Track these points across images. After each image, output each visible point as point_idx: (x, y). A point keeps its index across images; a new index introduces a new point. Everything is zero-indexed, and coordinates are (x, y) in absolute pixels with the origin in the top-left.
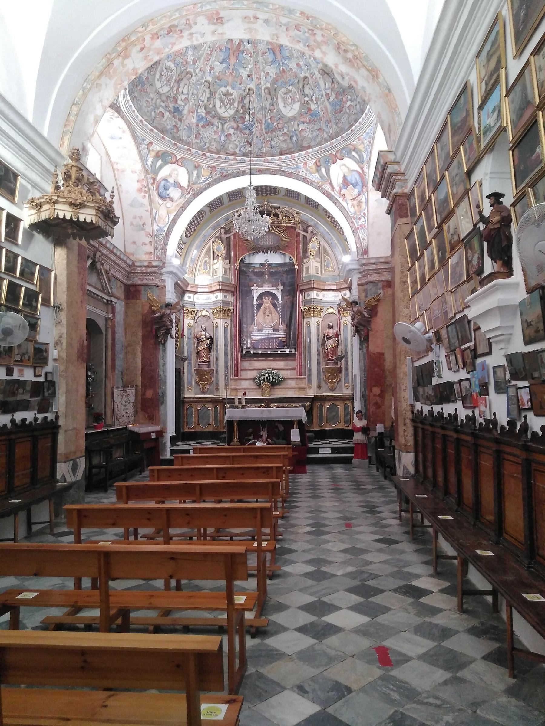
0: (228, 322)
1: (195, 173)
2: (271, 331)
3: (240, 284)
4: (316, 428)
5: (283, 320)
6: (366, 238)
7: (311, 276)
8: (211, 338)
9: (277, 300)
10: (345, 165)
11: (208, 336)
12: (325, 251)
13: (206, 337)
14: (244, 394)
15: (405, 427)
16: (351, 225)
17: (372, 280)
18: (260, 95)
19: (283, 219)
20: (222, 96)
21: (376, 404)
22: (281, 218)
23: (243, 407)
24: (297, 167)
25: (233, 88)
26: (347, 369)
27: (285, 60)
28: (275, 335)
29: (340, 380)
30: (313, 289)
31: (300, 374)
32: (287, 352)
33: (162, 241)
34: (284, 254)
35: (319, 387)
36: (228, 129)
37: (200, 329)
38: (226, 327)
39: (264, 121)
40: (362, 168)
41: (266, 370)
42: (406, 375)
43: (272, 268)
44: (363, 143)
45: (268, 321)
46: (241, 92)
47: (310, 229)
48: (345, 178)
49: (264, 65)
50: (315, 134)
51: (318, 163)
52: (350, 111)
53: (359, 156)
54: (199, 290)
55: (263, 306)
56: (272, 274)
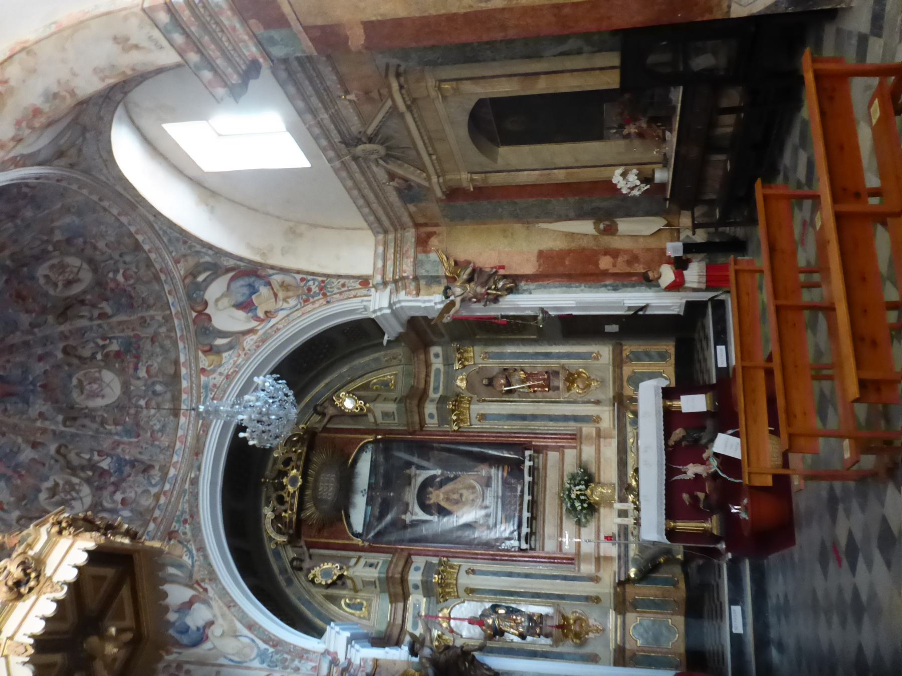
5: (470, 469)
10: (217, 300)
18: (73, 436)
20: (54, 499)
21: (629, 263)
25: (46, 479)
27: (26, 378)
33: (285, 656)
36: (114, 502)
39: (117, 438)
40: (228, 270)
43: (376, 483)
44: (185, 256)
46: (58, 466)
48: (239, 306)
49: (24, 417)
50: (158, 350)
51: (207, 348)
52: (132, 277)
53: (205, 270)
54: (399, 621)
55: (443, 504)
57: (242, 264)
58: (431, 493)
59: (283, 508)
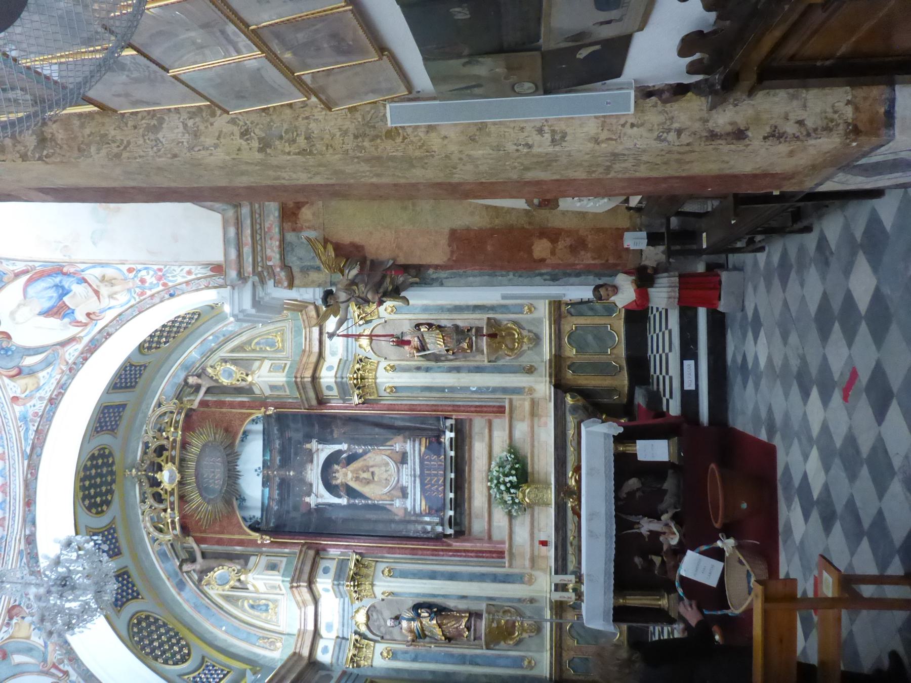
0: (381, 566)
1: (17, 659)
2: (406, 470)
3: (301, 533)
4: (623, 380)
6: (187, 268)
7: (288, 383)
8: (417, 607)
9: (339, 452)
10: (12, 314)
11: (410, 614)
12: (240, 348)
13: (413, 619)
14: (544, 543)
15: (755, 136)
16: (157, 300)
17: (278, 256)
19: (168, 438)
22: (165, 442)
23: (579, 580)
24: (24, 418)
26: (492, 308)
28: (414, 460)
29: (515, 322)
30: (315, 378)
31: (500, 410)
32: (453, 435)
34: (245, 434)
35: (530, 370)
37: (396, 631)
38: (392, 573)
40: (17, 275)
41: (490, 488)
42: (482, 127)
45: (385, 476)
47: (192, 380)
55: (353, 484)
56: (285, 462)
57: (37, 264)
58: (337, 471)
59: (162, 506)
